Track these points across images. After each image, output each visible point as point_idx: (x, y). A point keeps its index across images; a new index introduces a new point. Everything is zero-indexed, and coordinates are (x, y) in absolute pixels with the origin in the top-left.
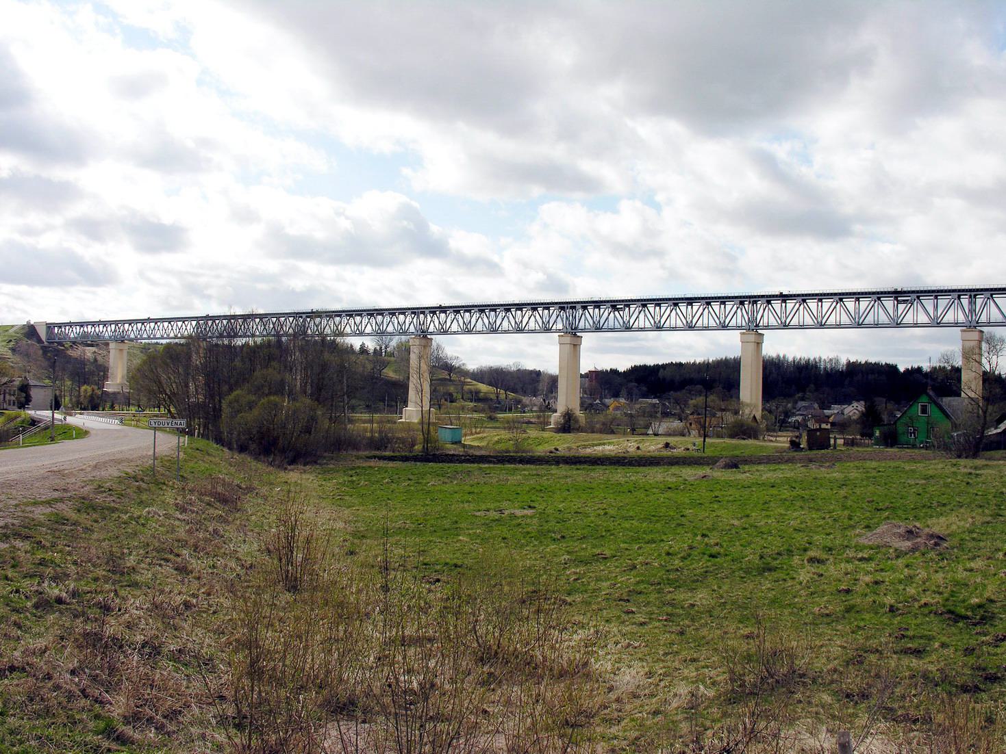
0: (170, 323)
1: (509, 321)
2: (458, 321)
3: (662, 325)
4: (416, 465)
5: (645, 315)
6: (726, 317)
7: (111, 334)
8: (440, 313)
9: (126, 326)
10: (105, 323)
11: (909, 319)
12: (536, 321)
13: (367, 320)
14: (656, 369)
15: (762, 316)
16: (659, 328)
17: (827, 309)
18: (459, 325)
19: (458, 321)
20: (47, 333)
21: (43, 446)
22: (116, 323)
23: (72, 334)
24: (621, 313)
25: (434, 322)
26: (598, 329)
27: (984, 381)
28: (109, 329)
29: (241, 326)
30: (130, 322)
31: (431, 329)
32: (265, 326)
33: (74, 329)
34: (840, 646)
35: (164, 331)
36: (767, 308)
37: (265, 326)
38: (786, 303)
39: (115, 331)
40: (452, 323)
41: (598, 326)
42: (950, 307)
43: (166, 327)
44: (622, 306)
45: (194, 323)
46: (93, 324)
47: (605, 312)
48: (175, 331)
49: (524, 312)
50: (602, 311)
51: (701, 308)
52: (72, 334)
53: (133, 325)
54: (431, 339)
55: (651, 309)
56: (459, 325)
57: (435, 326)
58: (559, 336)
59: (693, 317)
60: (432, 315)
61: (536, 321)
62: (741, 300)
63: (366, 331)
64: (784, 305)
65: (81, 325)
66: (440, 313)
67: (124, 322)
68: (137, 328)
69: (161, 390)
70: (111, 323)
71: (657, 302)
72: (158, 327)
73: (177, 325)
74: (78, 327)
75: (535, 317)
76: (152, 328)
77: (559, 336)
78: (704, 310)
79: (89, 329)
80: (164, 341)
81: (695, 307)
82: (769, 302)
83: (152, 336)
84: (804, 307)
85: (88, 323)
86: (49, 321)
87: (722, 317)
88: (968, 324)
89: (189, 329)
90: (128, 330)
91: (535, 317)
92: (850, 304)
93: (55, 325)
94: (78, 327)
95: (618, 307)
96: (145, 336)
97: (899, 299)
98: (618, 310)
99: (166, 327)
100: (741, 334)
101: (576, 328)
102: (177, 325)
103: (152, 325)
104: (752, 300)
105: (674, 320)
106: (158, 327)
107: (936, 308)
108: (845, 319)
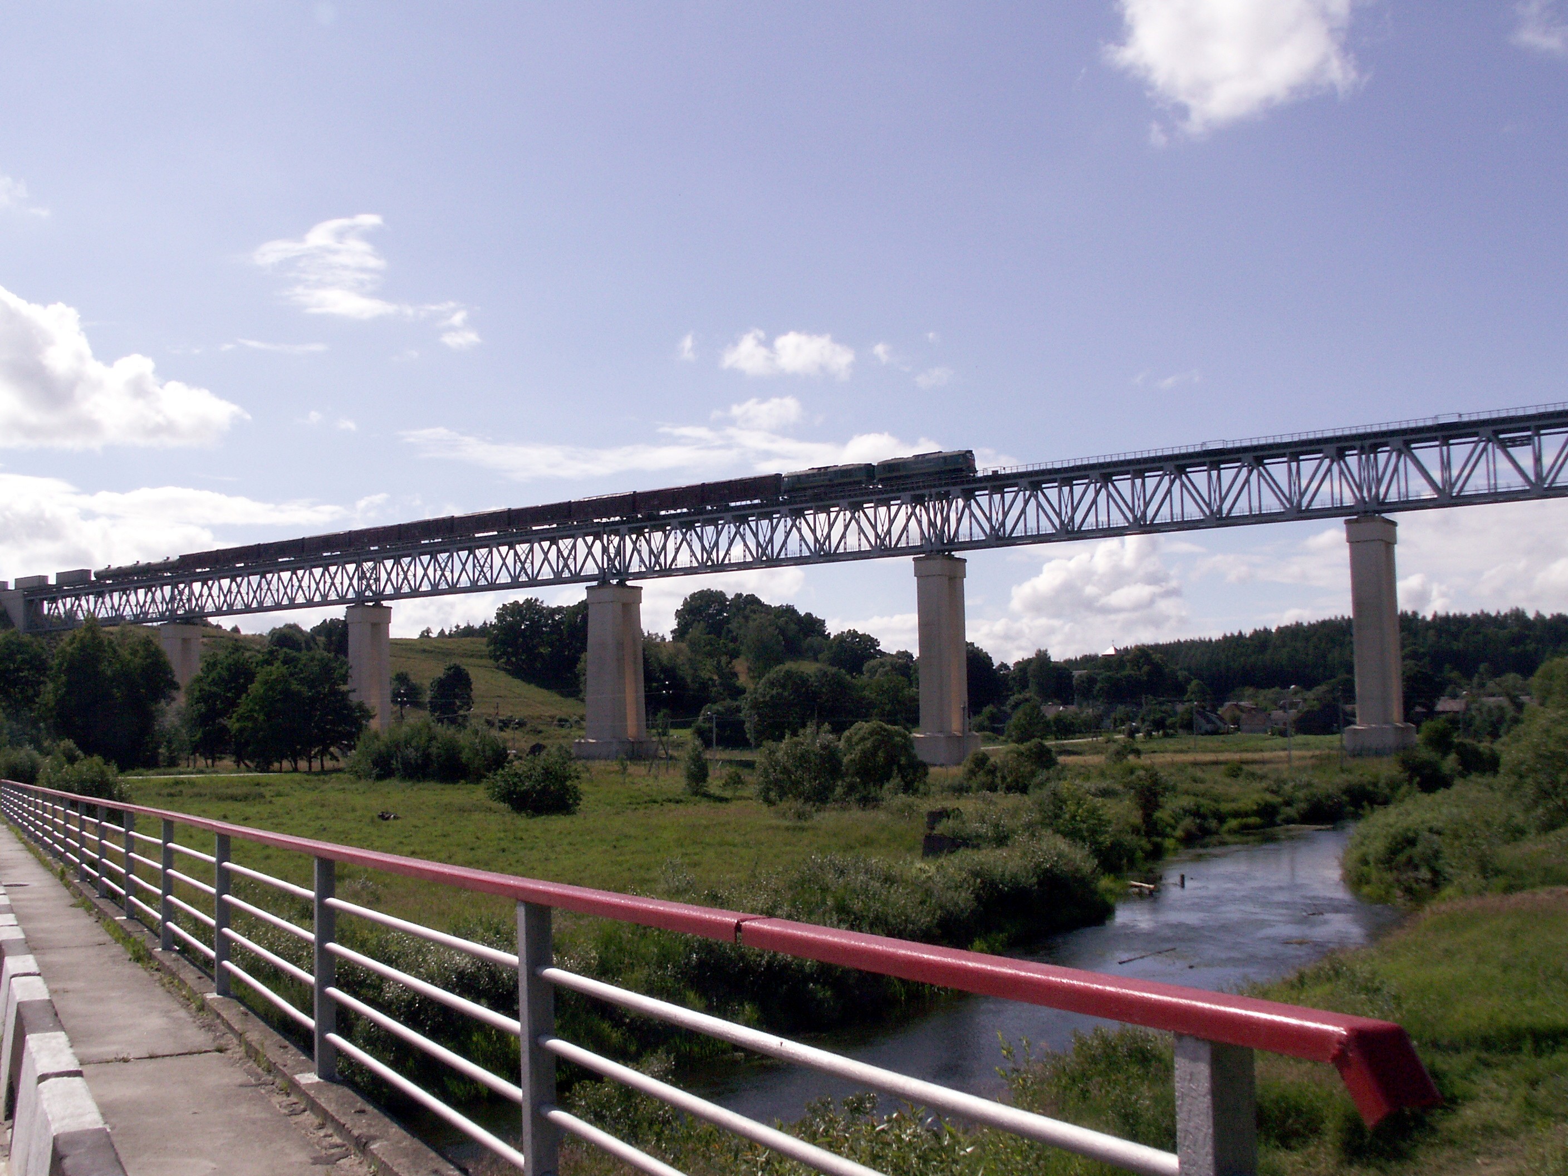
1: (746, 545)
2: (690, 547)
3: (1008, 532)
4: (1204, 1096)
5: (1039, 505)
6: (1147, 505)
8: (702, 527)
11: (1478, 483)
12: (861, 530)
13: (680, 537)
16: (1003, 538)
17: (1229, 483)
18: (693, 554)
19: (690, 547)
23: (128, 608)
25: (639, 552)
27: (1402, 629)
29: (318, 584)
31: (634, 568)
32: (443, 570)
33: (83, 602)
37: (443, 570)
38: (1143, 478)
39: (173, 598)
40: (787, 537)
42: (1406, 469)
48: (274, 592)
50: (894, 509)
52: (128, 608)
53: (210, 583)
55: (984, 501)
56: (693, 554)
57: (642, 560)
59: (1074, 510)
60: (634, 537)
61: (802, 538)
63: (423, 589)
64: (1214, 473)
66: (702, 527)
69: (342, 837)
71: (1104, 471)
72: (269, 584)
73: (249, 583)
74: (92, 598)
75: (799, 530)
78: (1026, 502)
81: (1151, 483)
82: (1407, 444)
84: (1183, 485)
88: (1361, 508)
90: (201, 595)
91: (858, 523)
92: (1199, 477)
97: (1502, 436)
100: (1347, 522)
101: (951, 541)
104: (1367, 443)
105: (1035, 521)
107: (1446, 465)
108: (1271, 504)
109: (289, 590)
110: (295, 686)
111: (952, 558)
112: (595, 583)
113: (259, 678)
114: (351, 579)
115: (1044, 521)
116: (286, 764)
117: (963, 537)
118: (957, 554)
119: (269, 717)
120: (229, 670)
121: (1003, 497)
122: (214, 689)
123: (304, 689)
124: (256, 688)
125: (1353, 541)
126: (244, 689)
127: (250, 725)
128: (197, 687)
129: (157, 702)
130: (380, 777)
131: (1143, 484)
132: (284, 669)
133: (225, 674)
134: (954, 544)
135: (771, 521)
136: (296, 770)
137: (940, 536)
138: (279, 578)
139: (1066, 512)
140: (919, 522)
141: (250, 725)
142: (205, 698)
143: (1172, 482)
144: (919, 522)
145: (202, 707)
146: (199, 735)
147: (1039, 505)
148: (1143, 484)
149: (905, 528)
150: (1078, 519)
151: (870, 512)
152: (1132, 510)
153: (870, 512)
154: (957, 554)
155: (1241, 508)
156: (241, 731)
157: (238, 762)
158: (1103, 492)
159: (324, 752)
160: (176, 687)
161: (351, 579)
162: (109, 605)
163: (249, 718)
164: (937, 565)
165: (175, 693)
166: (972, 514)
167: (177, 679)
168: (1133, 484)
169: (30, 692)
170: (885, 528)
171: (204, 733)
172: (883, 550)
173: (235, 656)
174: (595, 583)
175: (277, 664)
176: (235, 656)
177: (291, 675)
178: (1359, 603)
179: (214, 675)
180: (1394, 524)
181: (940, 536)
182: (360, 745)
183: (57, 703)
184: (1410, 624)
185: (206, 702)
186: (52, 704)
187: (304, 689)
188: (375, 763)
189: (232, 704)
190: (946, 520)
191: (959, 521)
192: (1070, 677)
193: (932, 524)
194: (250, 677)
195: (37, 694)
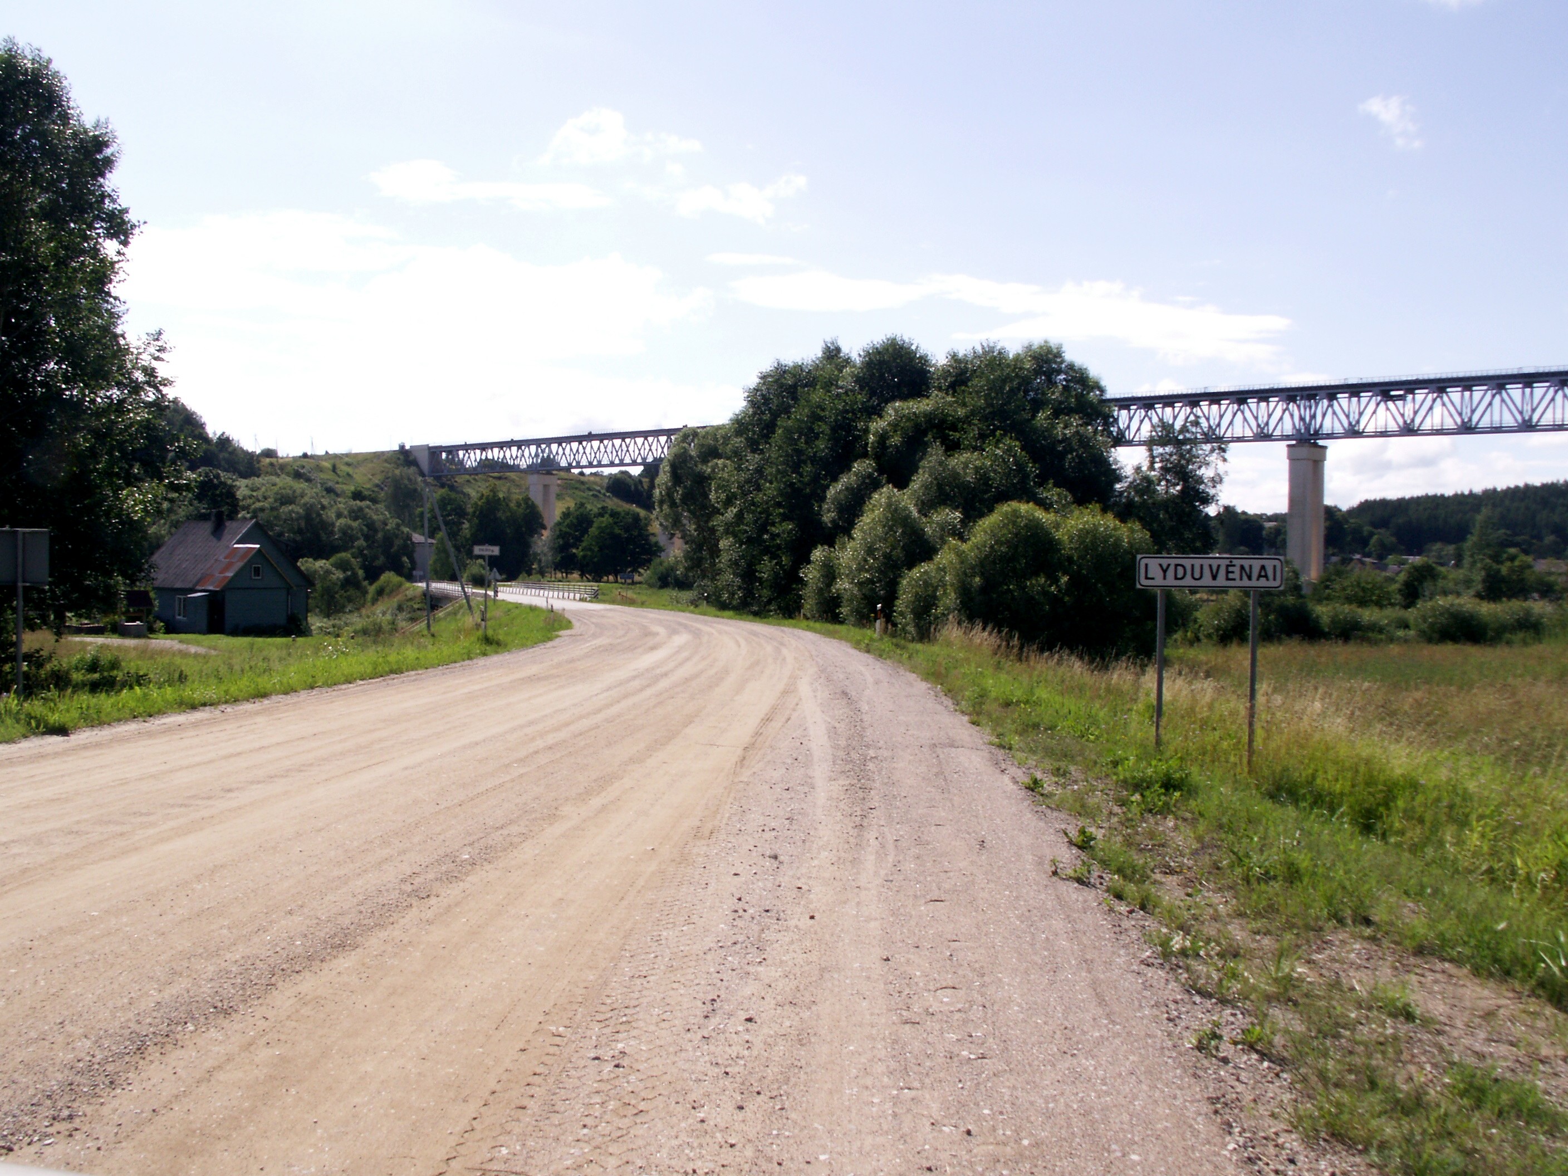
0: (580, 443)
6: (1473, 411)
7: (530, 462)
9: (554, 447)
10: (520, 444)
14: (1402, 505)
15: (1231, 423)
20: (431, 462)
21: (47, 563)
22: (538, 442)
24: (1399, 403)
26: (1353, 432)
28: (526, 453)
30: (560, 441)
34: (1456, 1028)
35: (615, 453)
36: (1330, 410)
39: (537, 455)
41: (1265, 431)
43: (617, 447)
44: (1401, 393)
45: (663, 439)
46: (501, 445)
47: (1276, 406)
49: (1132, 412)
51: (1552, 390)
53: (564, 445)
54: (1325, 448)
58: (1288, 446)
62: (1291, 395)
65: (483, 447)
67: (549, 441)
68: (571, 450)
70: (528, 443)
71: (1291, 393)
72: (584, 448)
76: (596, 450)
77: (1288, 446)
79: (495, 454)
80: (607, 471)
81: (1477, 395)
83: (574, 464)
85: (491, 446)
86: (432, 443)
87: (1466, 412)
89: (659, 449)
90: (557, 453)
92: (1515, 391)
93: (440, 449)
94: (478, 452)
95: (1393, 393)
96: (584, 462)
98: (1393, 398)
99: (617, 447)
102: (613, 445)
103: (596, 444)
106: (584, 448)
109: (642, 452)
110: (617, 531)
111: (1316, 445)
112: (1294, 442)
113: (595, 525)
114: (663, 448)
115: (1337, 425)
116: (611, 578)
117: (1327, 429)
118: (1321, 442)
119: (601, 549)
120: (577, 518)
121: (1359, 401)
122: (568, 530)
123: (622, 533)
124: (593, 531)
125: (1292, 459)
126: (585, 531)
127: (589, 553)
128: (557, 529)
129: (533, 537)
130: (661, 587)
131: (1532, 393)
132: (611, 520)
133: (575, 521)
134: (1317, 434)
135: (1129, 410)
136: (616, 582)
137: (1308, 428)
138: (635, 443)
139: (1466, 412)
140: (1292, 416)
141: (589, 553)
142: (562, 535)
143: (1556, 392)
144: (1292, 416)
145: (561, 542)
146: (559, 558)
147: (1503, 400)
148: (1532, 393)
149: (1281, 419)
150: (1475, 419)
151: (1253, 406)
152: (1521, 413)
153: (1253, 406)
154: (1321, 442)
155: (1547, 420)
156: (584, 557)
157: (582, 575)
158: (1498, 397)
159: (635, 570)
160: (544, 527)
161: (663, 448)
162: (473, 459)
163: (590, 550)
164: (1304, 451)
165: (544, 532)
166: (1334, 413)
167: (545, 522)
168: (1523, 393)
169: (455, 529)
170: (1217, 422)
171: (562, 557)
172: (1263, 436)
173: (581, 510)
174: (1294, 442)
175: (607, 516)
176: (581, 510)
177: (615, 523)
178: (1293, 501)
179: (568, 521)
180: (1325, 448)
181: (1308, 428)
182: (652, 567)
183: (472, 535)
184: (1331, 512)
185: (563, 538)
186: (468, 536)
187: (622, 533)
188: (660, 579)
189: (579, 540)
190: (1313, 417)
191: (1324, 415)
192: (1261, 528)
193: (1302, 419)
194: (590, 523)
195: (460, 530)
